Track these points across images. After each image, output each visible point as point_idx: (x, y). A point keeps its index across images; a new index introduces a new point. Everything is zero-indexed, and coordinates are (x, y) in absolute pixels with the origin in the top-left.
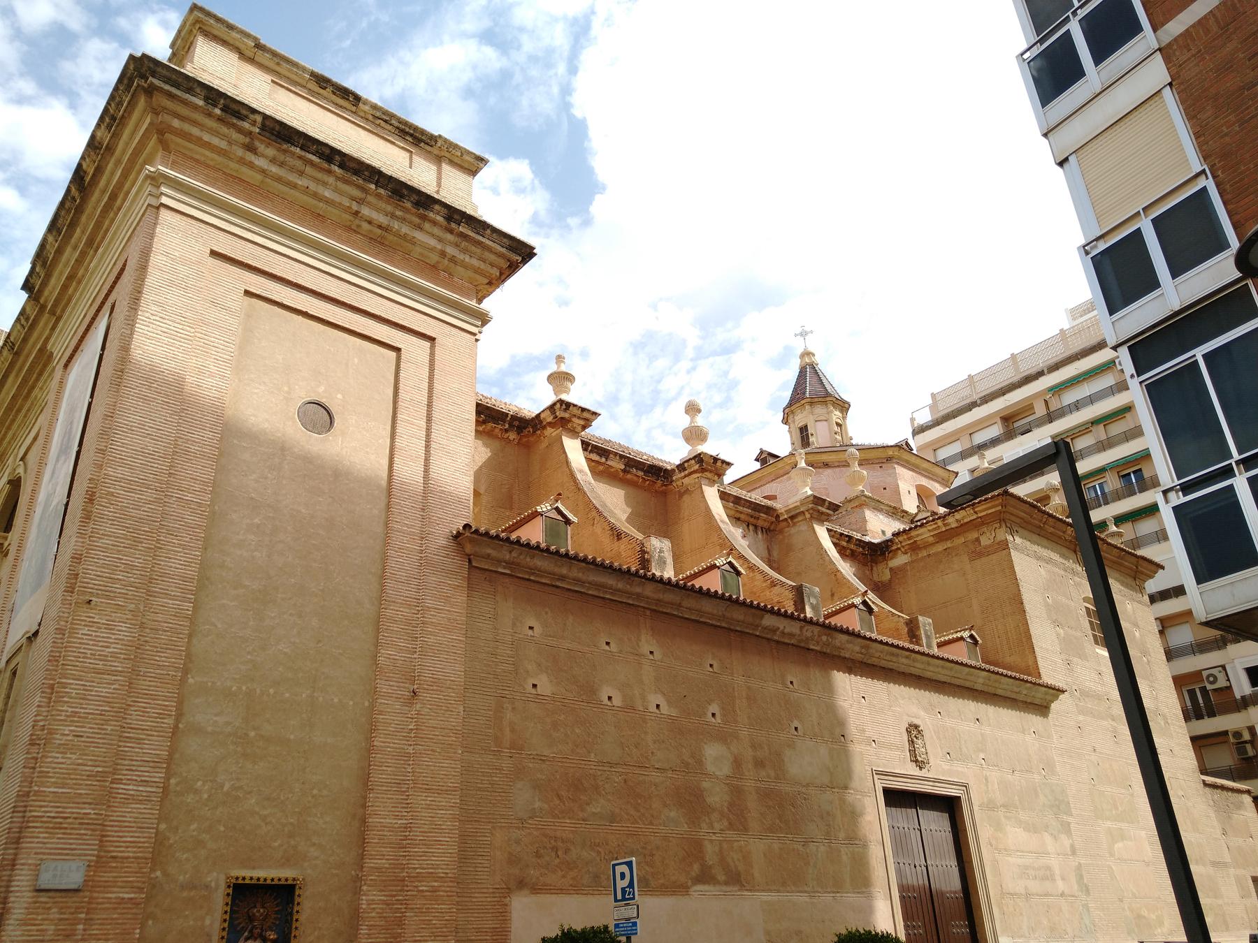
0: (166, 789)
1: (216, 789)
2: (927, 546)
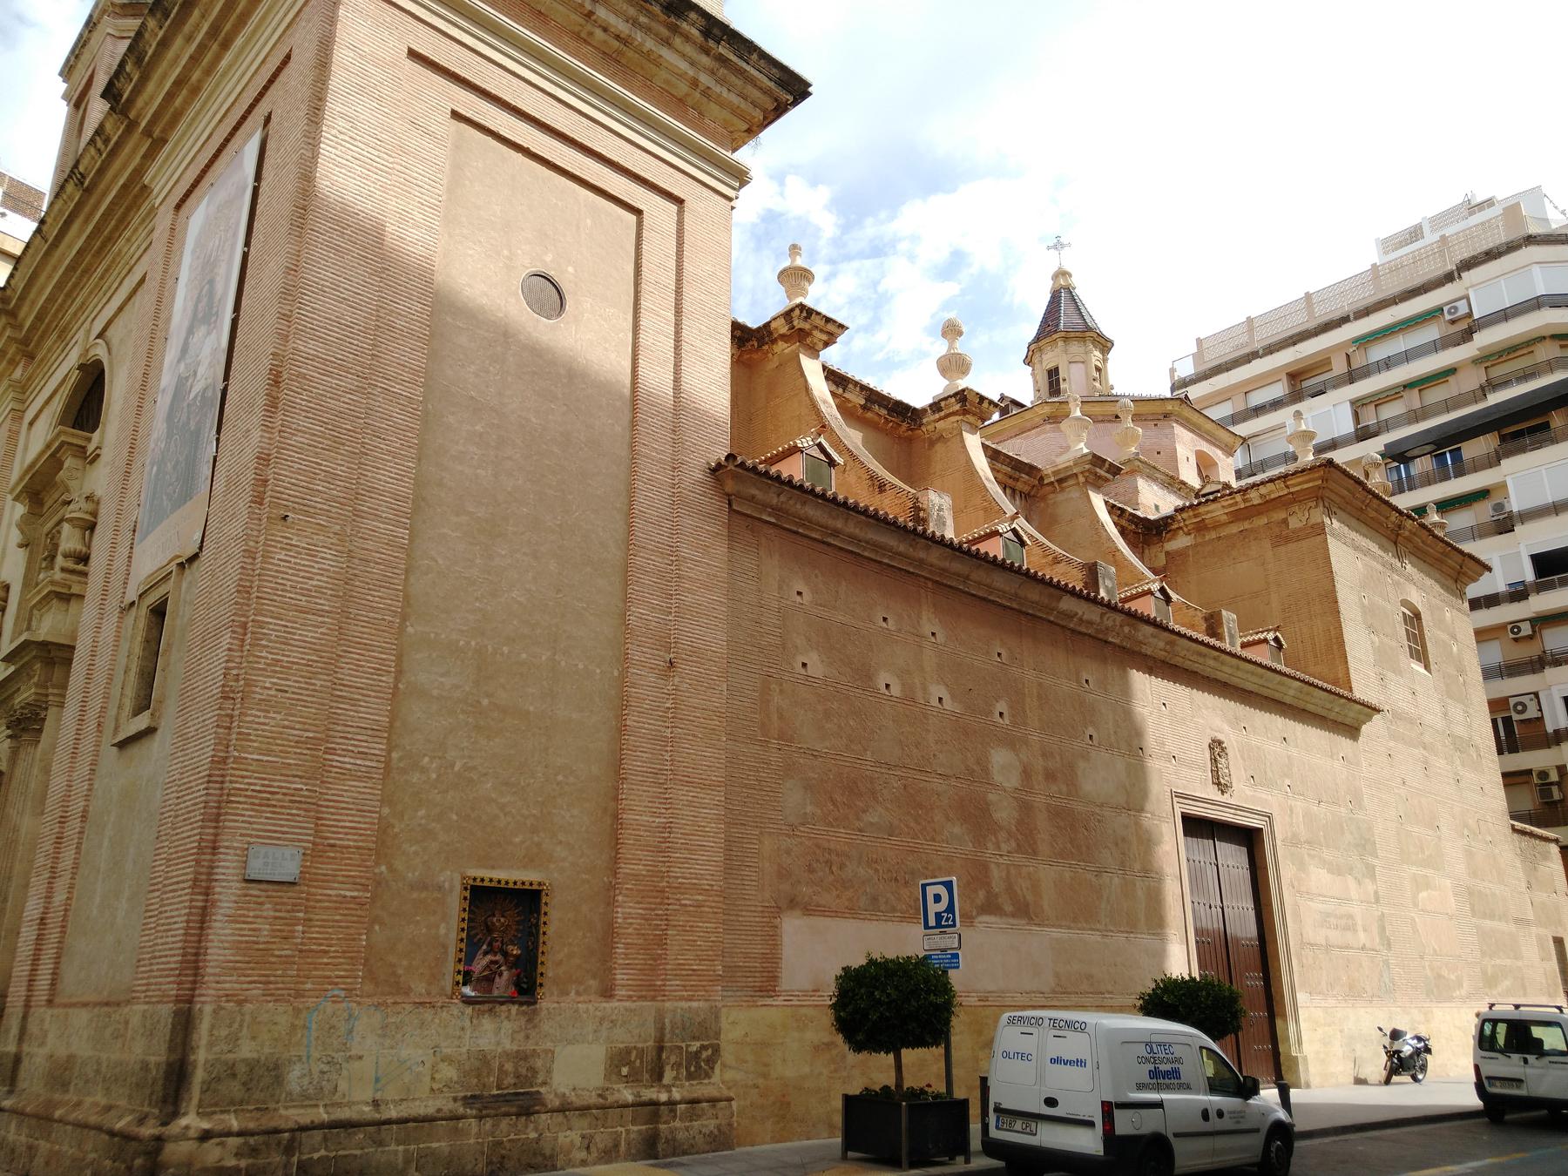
0: (388, 763)
1: (446, 768)
2: (1217, 525)
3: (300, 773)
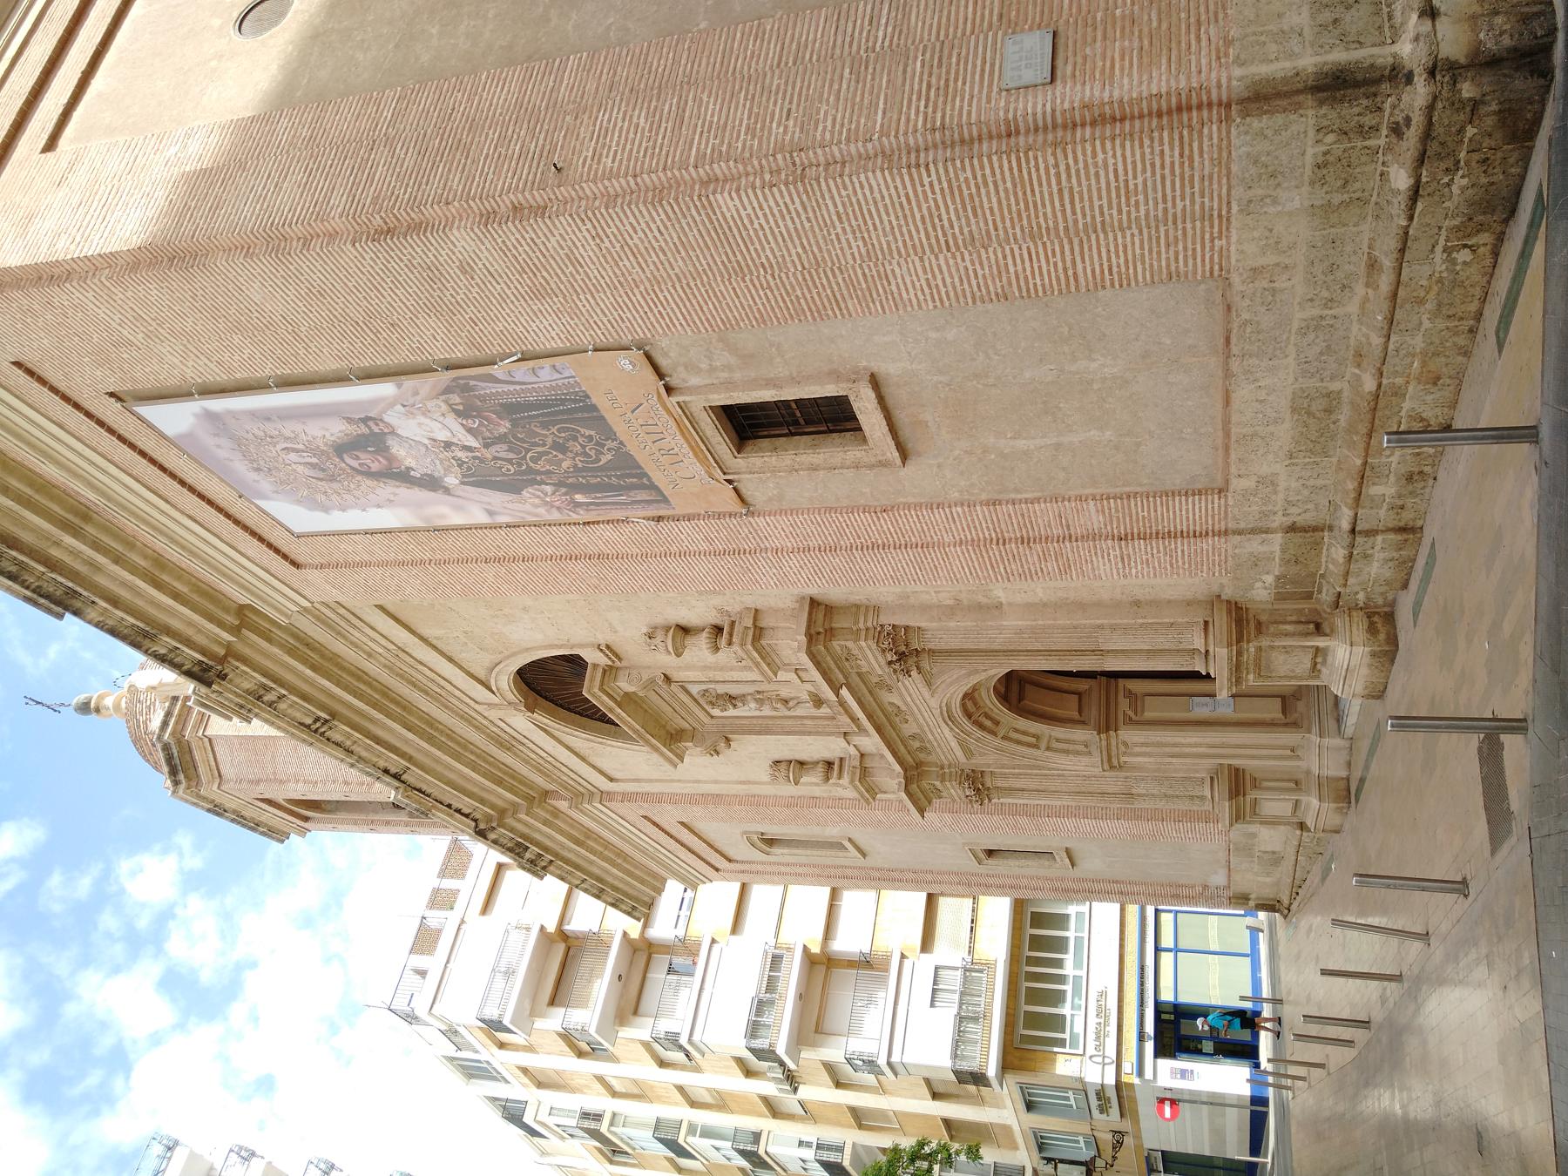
3: (901, 68)
